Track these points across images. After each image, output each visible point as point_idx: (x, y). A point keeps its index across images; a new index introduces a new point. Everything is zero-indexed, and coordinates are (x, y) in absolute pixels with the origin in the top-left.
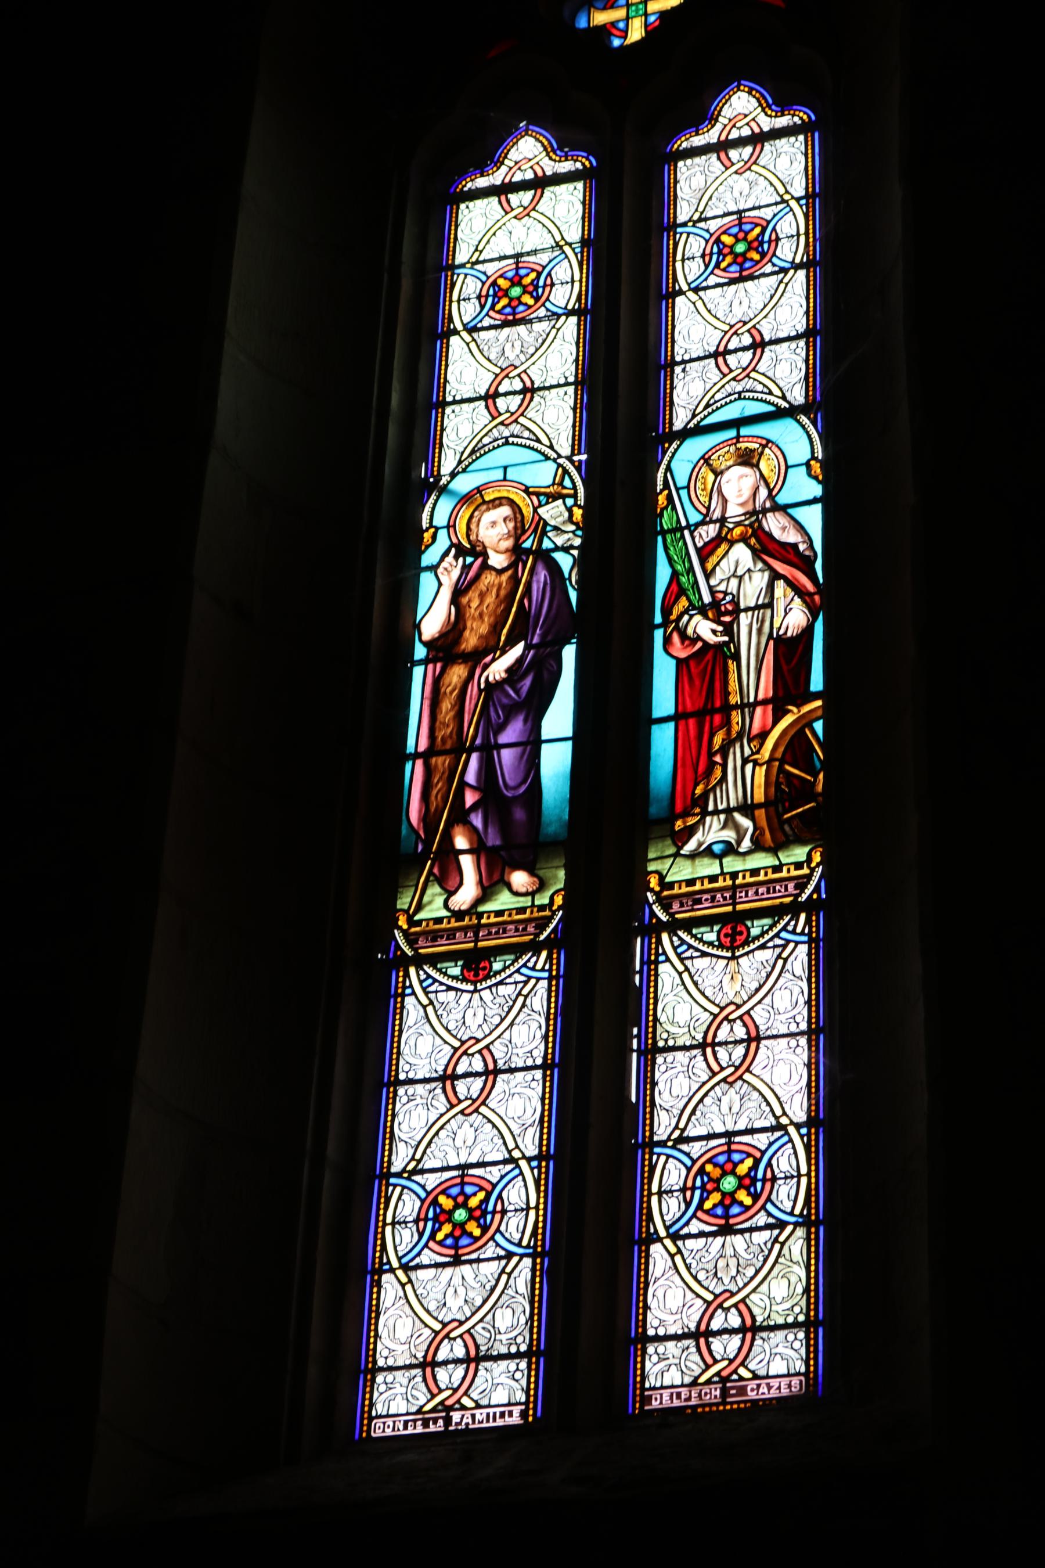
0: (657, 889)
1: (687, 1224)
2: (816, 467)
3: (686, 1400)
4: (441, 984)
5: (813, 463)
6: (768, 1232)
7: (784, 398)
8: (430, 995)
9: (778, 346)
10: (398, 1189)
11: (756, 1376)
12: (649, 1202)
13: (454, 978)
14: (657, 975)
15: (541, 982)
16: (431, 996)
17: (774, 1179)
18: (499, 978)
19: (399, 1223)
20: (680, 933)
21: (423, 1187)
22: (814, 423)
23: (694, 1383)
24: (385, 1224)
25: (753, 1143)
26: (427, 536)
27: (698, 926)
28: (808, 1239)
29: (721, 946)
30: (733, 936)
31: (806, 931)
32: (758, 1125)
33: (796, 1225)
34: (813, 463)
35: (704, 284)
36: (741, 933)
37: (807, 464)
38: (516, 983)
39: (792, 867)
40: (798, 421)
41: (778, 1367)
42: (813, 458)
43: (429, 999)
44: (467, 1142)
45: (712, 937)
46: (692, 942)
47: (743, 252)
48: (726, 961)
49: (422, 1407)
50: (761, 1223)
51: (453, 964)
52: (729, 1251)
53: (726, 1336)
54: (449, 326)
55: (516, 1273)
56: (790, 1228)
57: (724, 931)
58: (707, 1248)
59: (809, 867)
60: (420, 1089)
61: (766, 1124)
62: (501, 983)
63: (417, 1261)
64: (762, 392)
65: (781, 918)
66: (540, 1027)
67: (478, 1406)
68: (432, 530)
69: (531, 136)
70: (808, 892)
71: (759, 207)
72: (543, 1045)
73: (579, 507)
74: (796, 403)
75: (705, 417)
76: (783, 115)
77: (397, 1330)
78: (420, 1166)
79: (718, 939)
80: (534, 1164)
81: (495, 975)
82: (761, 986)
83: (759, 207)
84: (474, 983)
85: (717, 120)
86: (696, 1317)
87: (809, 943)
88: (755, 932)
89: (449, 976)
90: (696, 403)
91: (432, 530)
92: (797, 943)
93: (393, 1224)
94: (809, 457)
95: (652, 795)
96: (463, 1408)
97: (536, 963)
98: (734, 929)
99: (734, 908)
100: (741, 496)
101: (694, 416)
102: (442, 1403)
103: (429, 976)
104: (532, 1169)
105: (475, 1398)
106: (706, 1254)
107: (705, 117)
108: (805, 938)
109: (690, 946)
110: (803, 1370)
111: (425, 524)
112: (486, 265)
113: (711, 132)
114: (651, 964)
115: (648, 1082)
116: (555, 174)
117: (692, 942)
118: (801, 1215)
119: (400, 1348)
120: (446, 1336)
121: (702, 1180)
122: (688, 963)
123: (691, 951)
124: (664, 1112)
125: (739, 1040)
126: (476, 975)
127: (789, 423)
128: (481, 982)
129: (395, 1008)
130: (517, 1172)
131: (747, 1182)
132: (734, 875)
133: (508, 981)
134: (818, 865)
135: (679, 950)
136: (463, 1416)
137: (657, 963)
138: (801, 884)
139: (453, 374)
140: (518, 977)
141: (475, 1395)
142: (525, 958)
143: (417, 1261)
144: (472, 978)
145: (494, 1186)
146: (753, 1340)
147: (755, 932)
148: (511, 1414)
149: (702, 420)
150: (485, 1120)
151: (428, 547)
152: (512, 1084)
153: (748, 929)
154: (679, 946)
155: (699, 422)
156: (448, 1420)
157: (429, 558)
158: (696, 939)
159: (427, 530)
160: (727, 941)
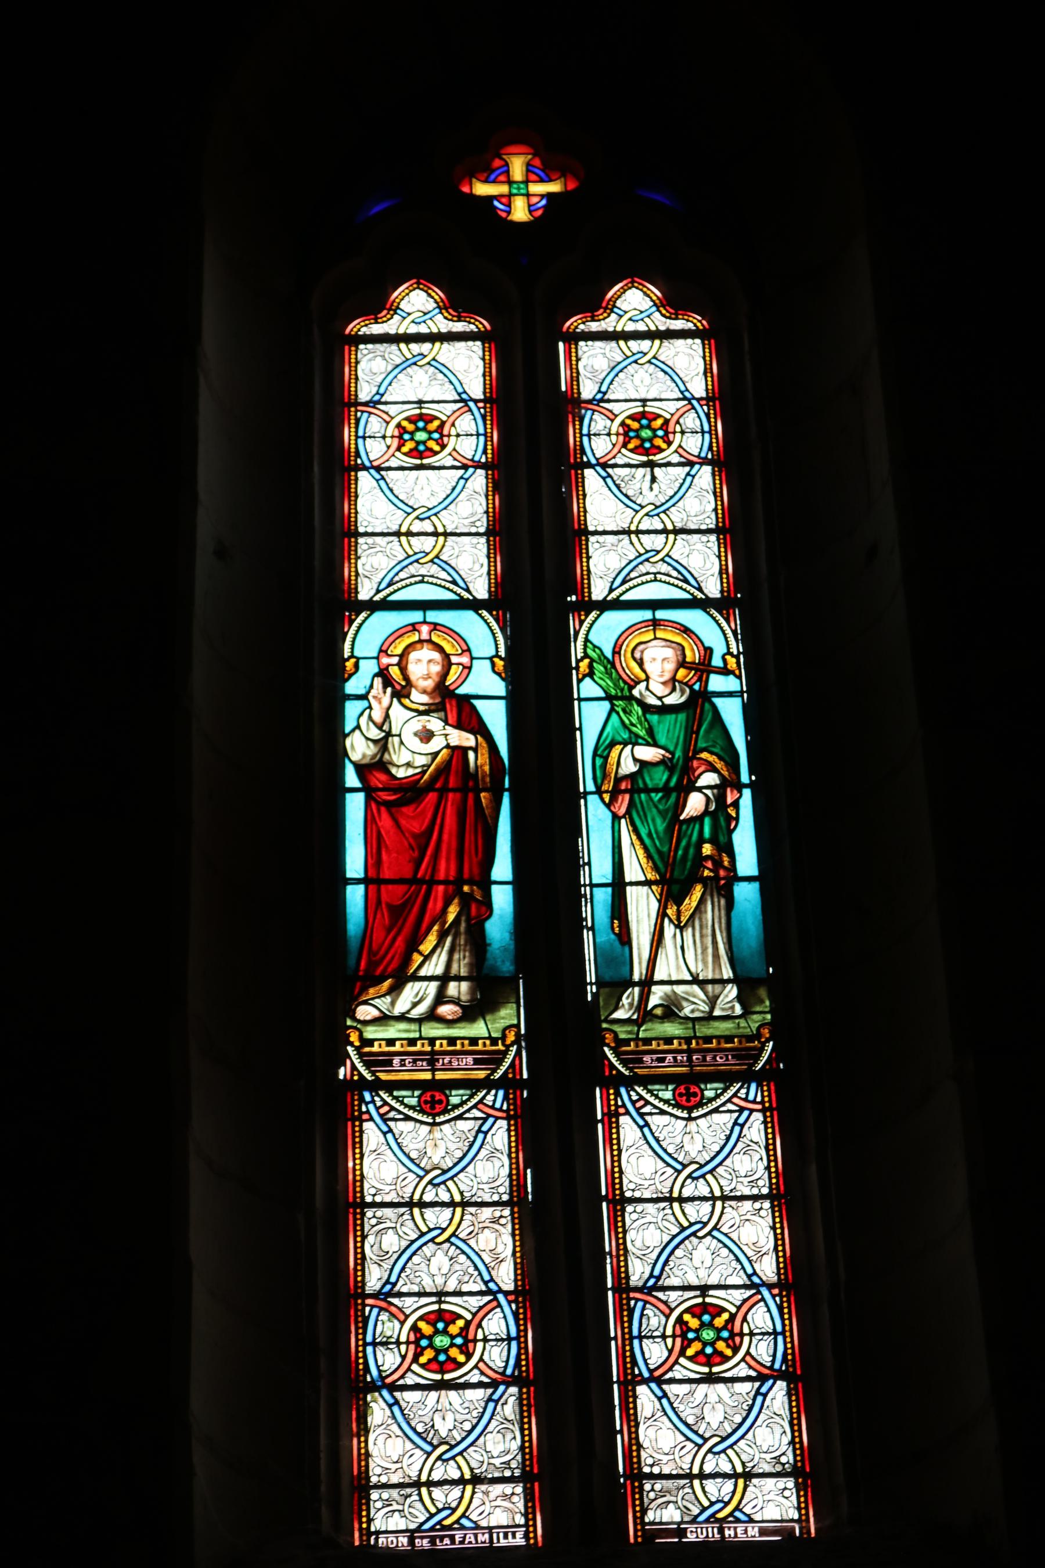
1: (670, 1369)
2: (500, 663)
3: (461, 1543)
5: (728, 657)
6: (482, 1391)
8: (389, 1123)
9: (689, 537)
10: (640, 1304)
11: (477, 1527)
12: (631, 1345)
13: (411, 1107)
15: (499, 1121)
18: (457, 1112)
20: (381, 1093)
24: (632, 1338)
25: (727, 1297)
26: (349, 665)
27: (399, 1089)
29: (678, 1106)
30: (433, 1103)
32: (730, 1281)
34: (728, 657)
35: (386, 465)
36: (695, 1095)
37: (491, 659)
38: (476, 1119)
39: (383, 1043)
40: (480, 615)
45: (413, 1101)
46: (393, 1103)
47: (421, 437)
48: (685, 1122)
50: (743, 1374)
51: (663, 1087)
53: (719, 1480)
54: (582, 458)
57: (423, 1099)
58: (691, 1393)
59: (503, 1044)
60: (388, 1212)
61: (475, 1288)
62: (716, 1110)
64: (677, 578)
65: (478, 1090)
66: (761, 1159)
67: (751, 1520)
68: (353, 660)
69: (637, 288)
70: (503, 1068)
71: (661, 400)
72: (766, 1175)
73: (500, 657)
74: (711, 596)
75: (624, 593)
76: (677, 319)
77: (387, 1449)
78: (660, 1283)
79: (419, 1105)
80: (776, 1291)
81: (453, 1110)
82: (465, 1155)
83: (661, 400)
84: (434, 1116)
86: (417, 1466)
88: (455, 1100)
89: (661, 1100)
90: (613, 576)
91: (353, 660)
92: (752, 1111)
94: (725, 651)
95: (488, 955)
97: (747, 1094)
98: (687, 1089)
99: (434, 1075)
100: (662, 676)
101: (378, 591)
102: (439, 1522)
103: (641, 1098)
104: (774, 1296)
105: (748, 1513)
108: (759, 1107)
109: (392, 1109)
110: (796, 1517)
111: (346, 655)
112: (612, 404)
113: (607, 320)
114: (612, 1116)
115: (619, 1229)
116: (668, 331)
117: (393, 1103)
121: (681, 1328)
122: (647, 1118)
125: (700, 1195)
127: (470, 614)
128: (439, 1114)
129: (354, 1132)
130: (494, 1304)
132: (432, 1041)
133: (467, 1115)
134: (512, 1044)
135: (638, 1105)
136: (465, 1535)
137: (617, 1115)
138: (493, 1059)
139: (363, 505)
140: (476, 1113)
142: (481, 1095)
144: (429, 1110)
147: (455, 1100)
150: (721, 1245)
151: (351, 676)
153: (447, 1097)
155: (618, 597)
157: (352, 687)
159: (348, 660)
160: (427, 1107)
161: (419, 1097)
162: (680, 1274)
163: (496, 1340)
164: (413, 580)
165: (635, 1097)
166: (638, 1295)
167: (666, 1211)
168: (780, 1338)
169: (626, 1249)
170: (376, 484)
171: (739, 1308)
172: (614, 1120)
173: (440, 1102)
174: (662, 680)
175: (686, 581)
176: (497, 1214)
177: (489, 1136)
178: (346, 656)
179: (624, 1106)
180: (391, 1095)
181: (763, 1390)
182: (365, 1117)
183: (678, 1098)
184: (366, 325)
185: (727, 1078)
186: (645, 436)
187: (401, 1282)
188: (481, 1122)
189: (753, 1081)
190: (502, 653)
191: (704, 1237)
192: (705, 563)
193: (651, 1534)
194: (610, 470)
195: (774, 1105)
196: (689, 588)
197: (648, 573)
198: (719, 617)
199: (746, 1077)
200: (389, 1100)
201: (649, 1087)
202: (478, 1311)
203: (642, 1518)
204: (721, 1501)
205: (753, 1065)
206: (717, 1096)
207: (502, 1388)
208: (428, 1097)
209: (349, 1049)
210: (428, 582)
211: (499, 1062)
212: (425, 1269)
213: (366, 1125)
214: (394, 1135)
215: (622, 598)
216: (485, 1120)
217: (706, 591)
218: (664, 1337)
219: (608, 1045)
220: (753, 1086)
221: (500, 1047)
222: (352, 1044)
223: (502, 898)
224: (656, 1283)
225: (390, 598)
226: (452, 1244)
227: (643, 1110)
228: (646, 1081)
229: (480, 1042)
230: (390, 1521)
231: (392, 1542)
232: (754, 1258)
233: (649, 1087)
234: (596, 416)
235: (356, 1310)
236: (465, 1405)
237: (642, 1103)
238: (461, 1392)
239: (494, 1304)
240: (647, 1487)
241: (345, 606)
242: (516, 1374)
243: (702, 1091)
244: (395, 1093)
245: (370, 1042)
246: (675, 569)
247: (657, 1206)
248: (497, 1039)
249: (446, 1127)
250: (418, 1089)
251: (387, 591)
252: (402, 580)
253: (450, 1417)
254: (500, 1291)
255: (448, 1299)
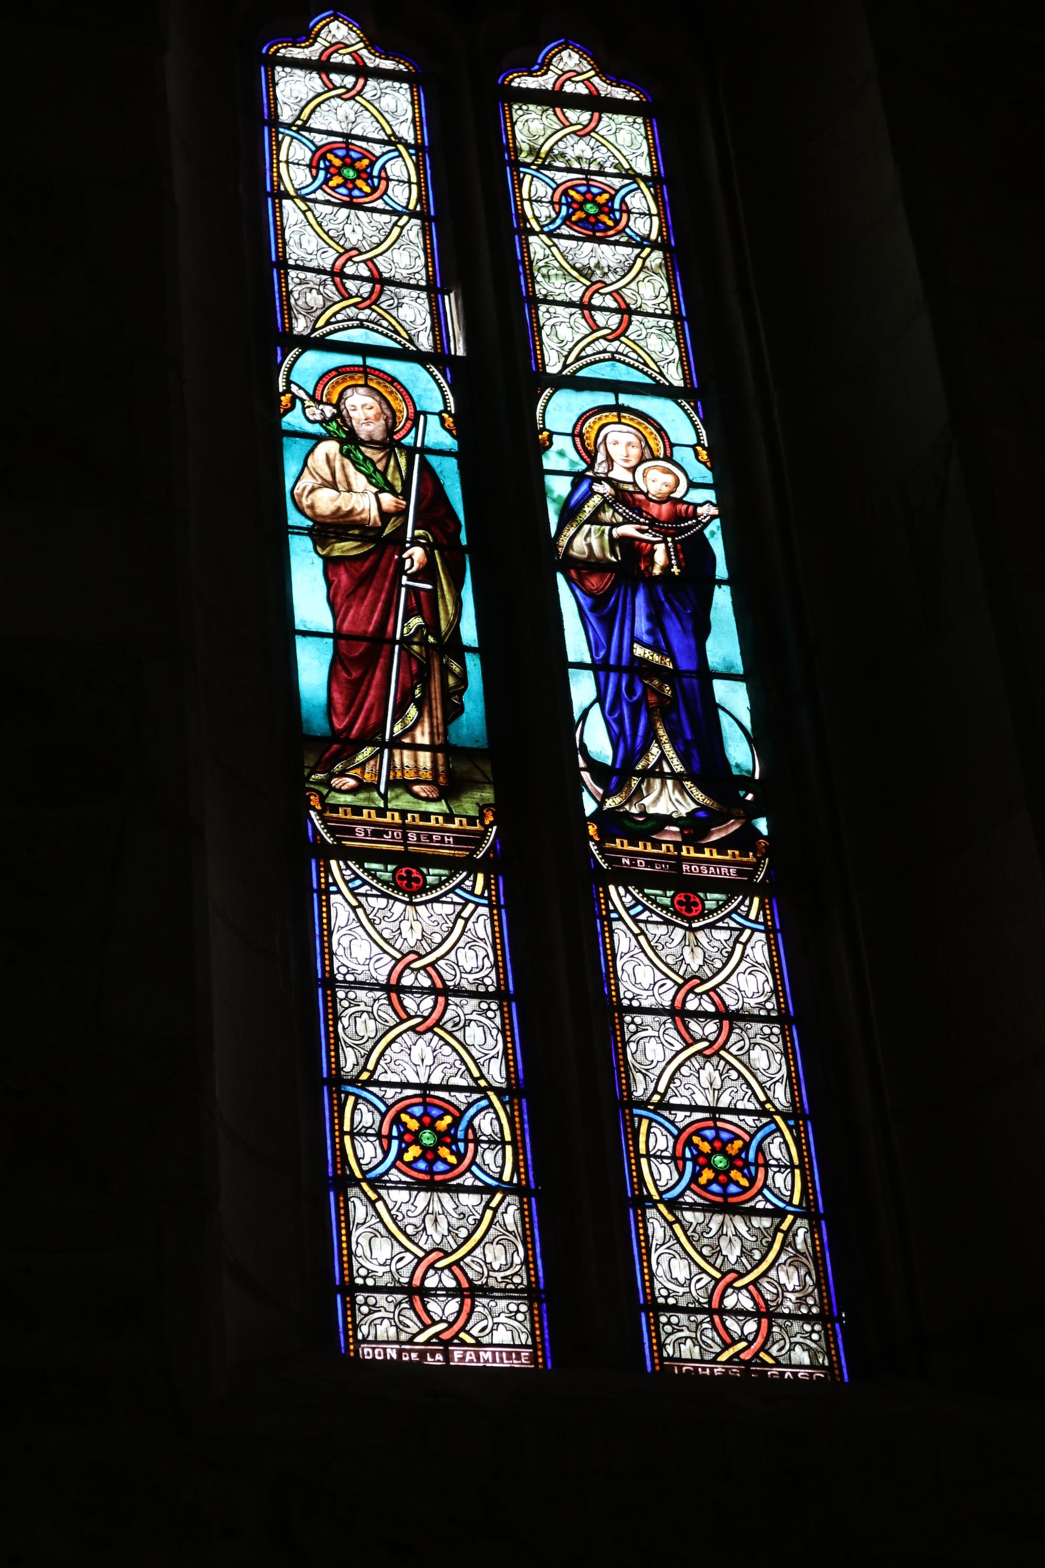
0: (319, 807)
2: (450, 421)
4: (373, 887)
7: (411, 341)
11: (479, 1344)
13: (384, 883)
14: (328, 906)
15: (480, 908)
16: (642, 925)
17: (674, 1158)
19: (786, 1167)
21: (673, 1123)
22: (445, 377)
23: (714, 1361)
24: (343, 1133)
26: (285, 399)
28: (521, 1209)
30: (689, 905)
31: (486, 894)
33: (797, 1216)
36: (695, 904)
41: (502, 1336)
42: (445, 411)
43: (640, 928)
44: (416, 1060)
46: (364, 876)
49: (415, 1335)
52: (731, 1231)
55: (502, 1209)
56: (790, 1218)
57: (677, 899)
59: (482, 823)
62: (436, 900)
63: (460, 1181)
66: (767, 980)
85: (315, 41)
87: (766, 931)
88: (710, 905)
93: (504, 1143)
96: (463, 1343)
100: (627, 461)
106: (413, 1208)
107: (305, 36)
109: (365, 883)
117: (364, 876)
118: (800, 1206)
119: (381, 1270)
120: (432, 1264)
123: (367, 887)
124: (350, 1049)
126: (689, 910)
131: (738, 1162)
132: (403, 813)
133: (444, 899)
134: (491, 825)
141: (475, 1332)
143: (460, 1181)
145: (463, 1113)
146: (770, 1327)
147: (710, 905)
148: (518, 1357)
149: (332, 332)
152: (467, 1009)
154: (352, 880)
156: (447, 1356)
158: (649, 899)
161: (394, 872)
162: (399, 1069)
163: (662, 1157)
164: (350, 323)
165: (628, 899)
166: (350, 1089)
167: (382, 1001)
168: (797, 1172)
169: (337, 1037)
170: (302, 217)
171: (752, 1137)
172: (324, 898)
173: (417, 880)
174: (628, 465)
175: (396, 332)
176: (484, 1006)
177: (749, 947)
178: (281, 390)
179: (335, 884)
180: (361, 866)
181: (493, 1204)
182: (333, 889)
183: (677, 906)
184: (285, 47)
185: (453, 865)
186: (348, 169)
187: (380, 1070)
188: (737, 933)
189: (757, 895)
190: (452, 409)
191: (424, 1032)
192: (662, 348)
193: (667, 1366)
194: (555, 240)
195: (778, 927)
196: (399, 339)
197: (605, 351)
198: (436, 372)
199: (472, 867)
200: (359, 872)
201: (646, 891)
202: (756, 1133)
203: (660, 1351)
204: (446, 1321)
205: (474, 852)
206: (719, 908)
207: (499, 1196)
208: (681, 897)
209: (312, 813)
210: (367, 328)
211: (479, 844)
212: (407, 1059)
213: (334, 898)
214: (365, 910)
215: (578, 374)
216: (464, 906)
217: (417, 344)
218: (477, 1142)
219: (315, 810)
220: (480, 877)
221: (478, 827)
222: (314, 808)
223: (733, 699)
224: (371, 1076)
225: (580, 374)
226: (436, 1034)
227: (640, 917)
228: (362, 856)
229: (433, 817)
230: (382, 1330)
231: (368, 1354)
232: (768, 1085)
233: (646, 891)
234: (295, 142)
235: (625, 1121)
236: (459, 1210)
237: (358, 882)
238: (454, 1195)
239: (773, 1126)
240: (360, 1299)
241: (270, 337)
242: (515, 1181)
243: (702, 901)
244: (366, 865)
245: (335, 808)
246: (634, 351)
247: (370, 994)
248: (475, 818)
249: (421, 909)
250: (392, 864)
251: (577, 365)
252: (588, 356)
253: (443, 1221)
254: (490, 1087)
255: (723, 1116)
